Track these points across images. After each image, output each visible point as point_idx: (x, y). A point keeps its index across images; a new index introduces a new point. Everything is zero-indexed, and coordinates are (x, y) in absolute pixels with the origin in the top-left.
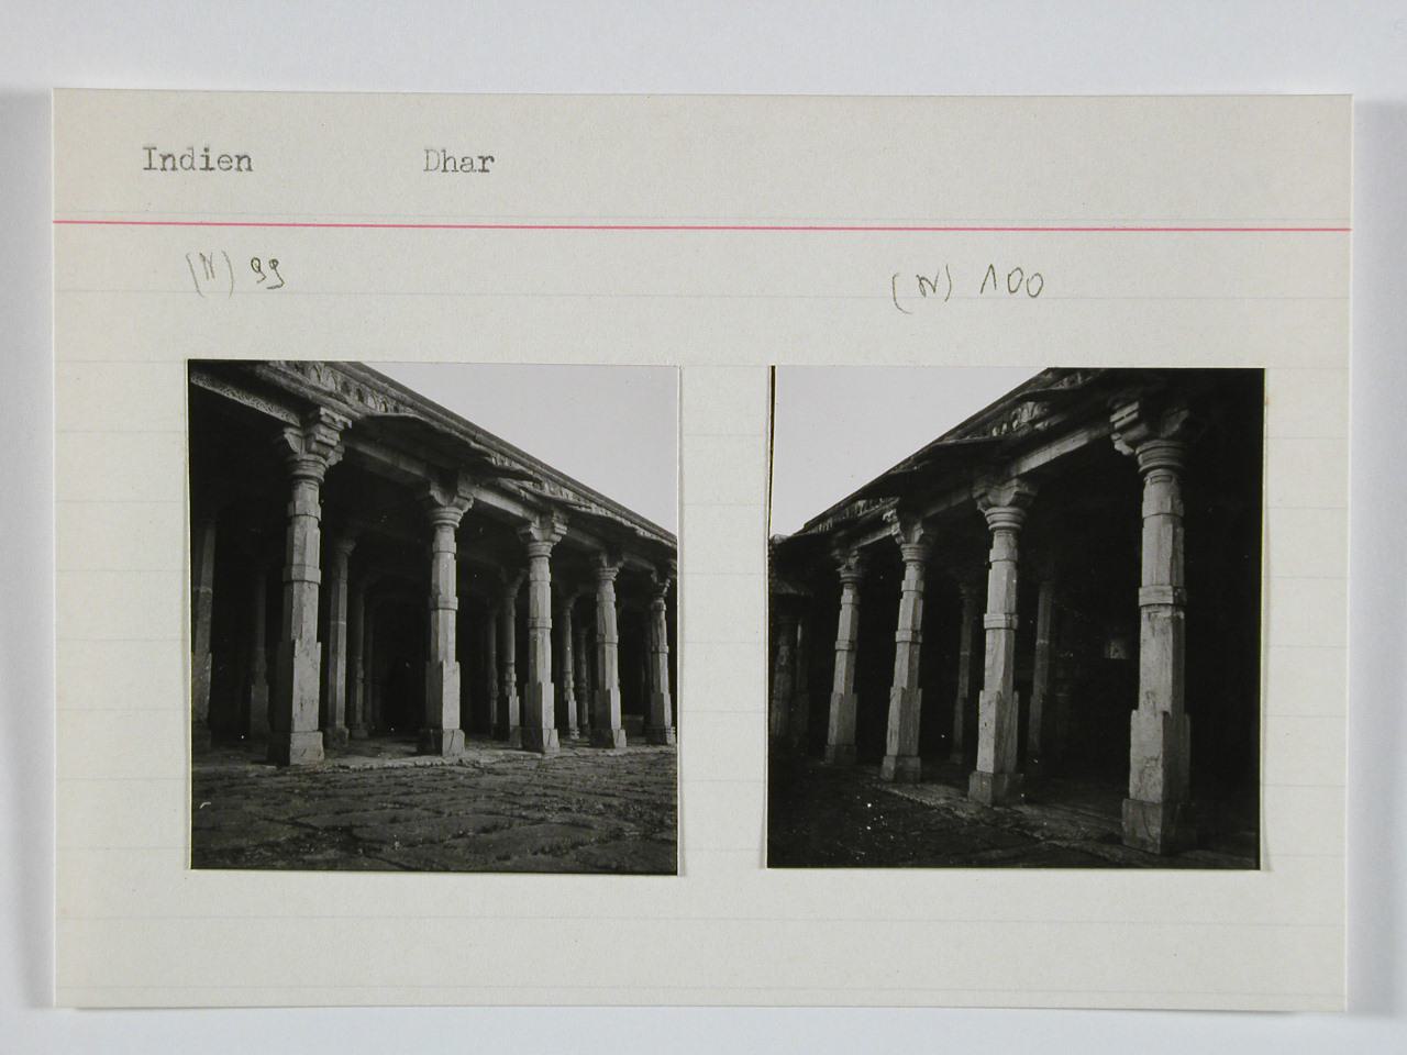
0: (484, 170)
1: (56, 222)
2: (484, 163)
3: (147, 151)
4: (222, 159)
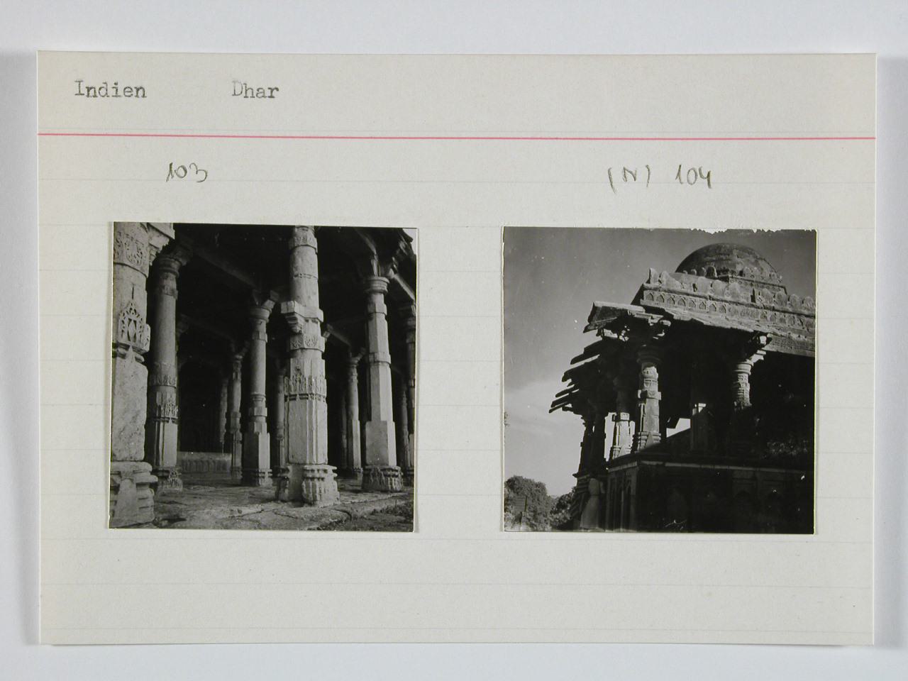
0: (271, 97)
1: (39, 134)
2: (272, 92)
3: (78, 83)
4: (127, 90)
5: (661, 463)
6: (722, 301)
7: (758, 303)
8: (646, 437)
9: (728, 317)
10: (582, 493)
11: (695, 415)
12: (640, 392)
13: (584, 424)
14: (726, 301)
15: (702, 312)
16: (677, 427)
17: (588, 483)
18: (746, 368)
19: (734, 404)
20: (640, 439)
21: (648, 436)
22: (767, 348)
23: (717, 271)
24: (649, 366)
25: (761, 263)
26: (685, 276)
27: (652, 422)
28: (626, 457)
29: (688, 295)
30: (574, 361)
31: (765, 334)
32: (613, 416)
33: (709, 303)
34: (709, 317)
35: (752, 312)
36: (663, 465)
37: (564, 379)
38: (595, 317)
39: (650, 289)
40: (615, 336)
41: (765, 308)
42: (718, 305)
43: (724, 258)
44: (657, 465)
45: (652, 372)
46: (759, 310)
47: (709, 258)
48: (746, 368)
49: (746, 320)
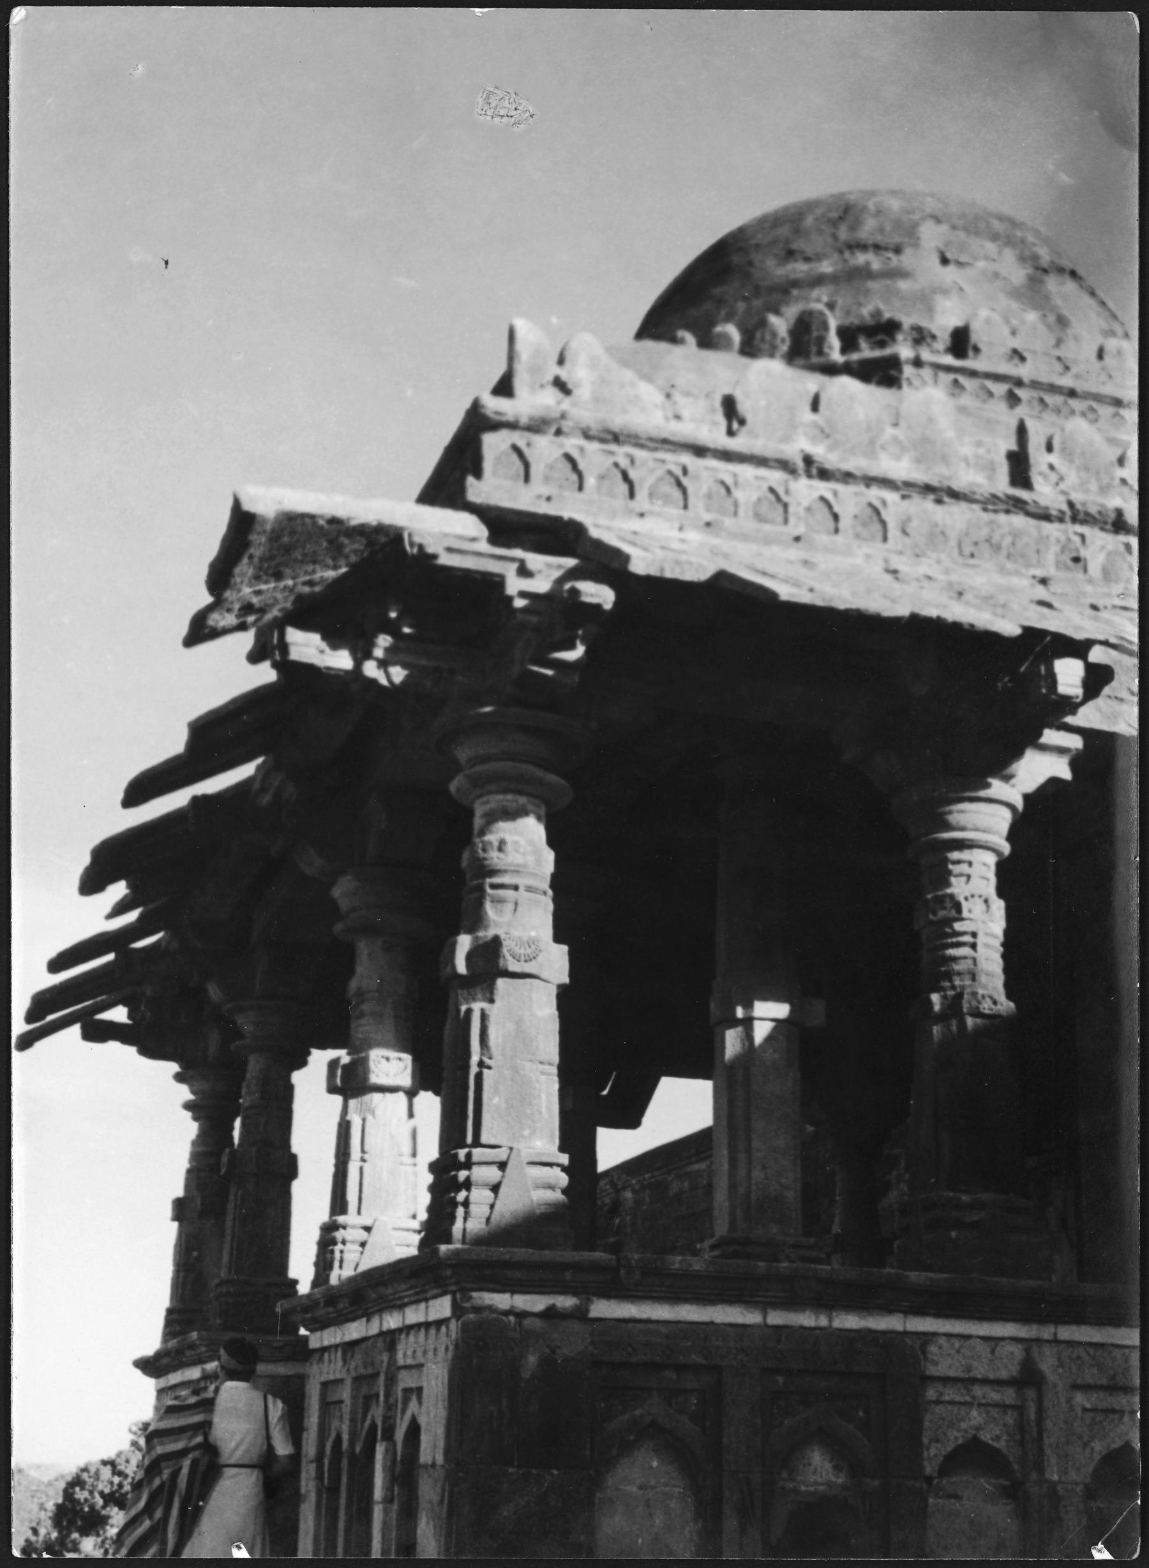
5: (566, 1302)
6: (870, 481)
7: (1044, 492)
8: (493, 1174)
9: (896, 562)
10: (183, 1453)
11: (738, 1059)
12: (464, 943)
13: (188, 1106)
14: (886, 483)
15: (768, 541)
16: (648, 1118)
17: (208, 1405)
18: (985, 822)
19: (930, 1003)
20: (467, 1185)
21: (502, 1166)
22: (1088, 716)
23: (843, 332)
24: (512, 814)
25: (1058, 289)
26: (682, 356)
27: (522, 1098)
28: (398, 1270)
29: (700, 451)
30: (139, 791)
31: (1078, 648)
32: (333, 1065)
33: (806, 490)
34: (806, 563)
35: (1016, 534)
36: (580, 1314)
37: (92, 883)
38: (244, 569)
39: (513, 426)
40: (342, 660)
41: (1077, 515)
42: (850, 500)
43: (876, 264)
44: (551, 1313)
45: (523, 847)
46: (1051, 529)
47: (799, 268)
48: (985, 822)
49: (982, 577)
